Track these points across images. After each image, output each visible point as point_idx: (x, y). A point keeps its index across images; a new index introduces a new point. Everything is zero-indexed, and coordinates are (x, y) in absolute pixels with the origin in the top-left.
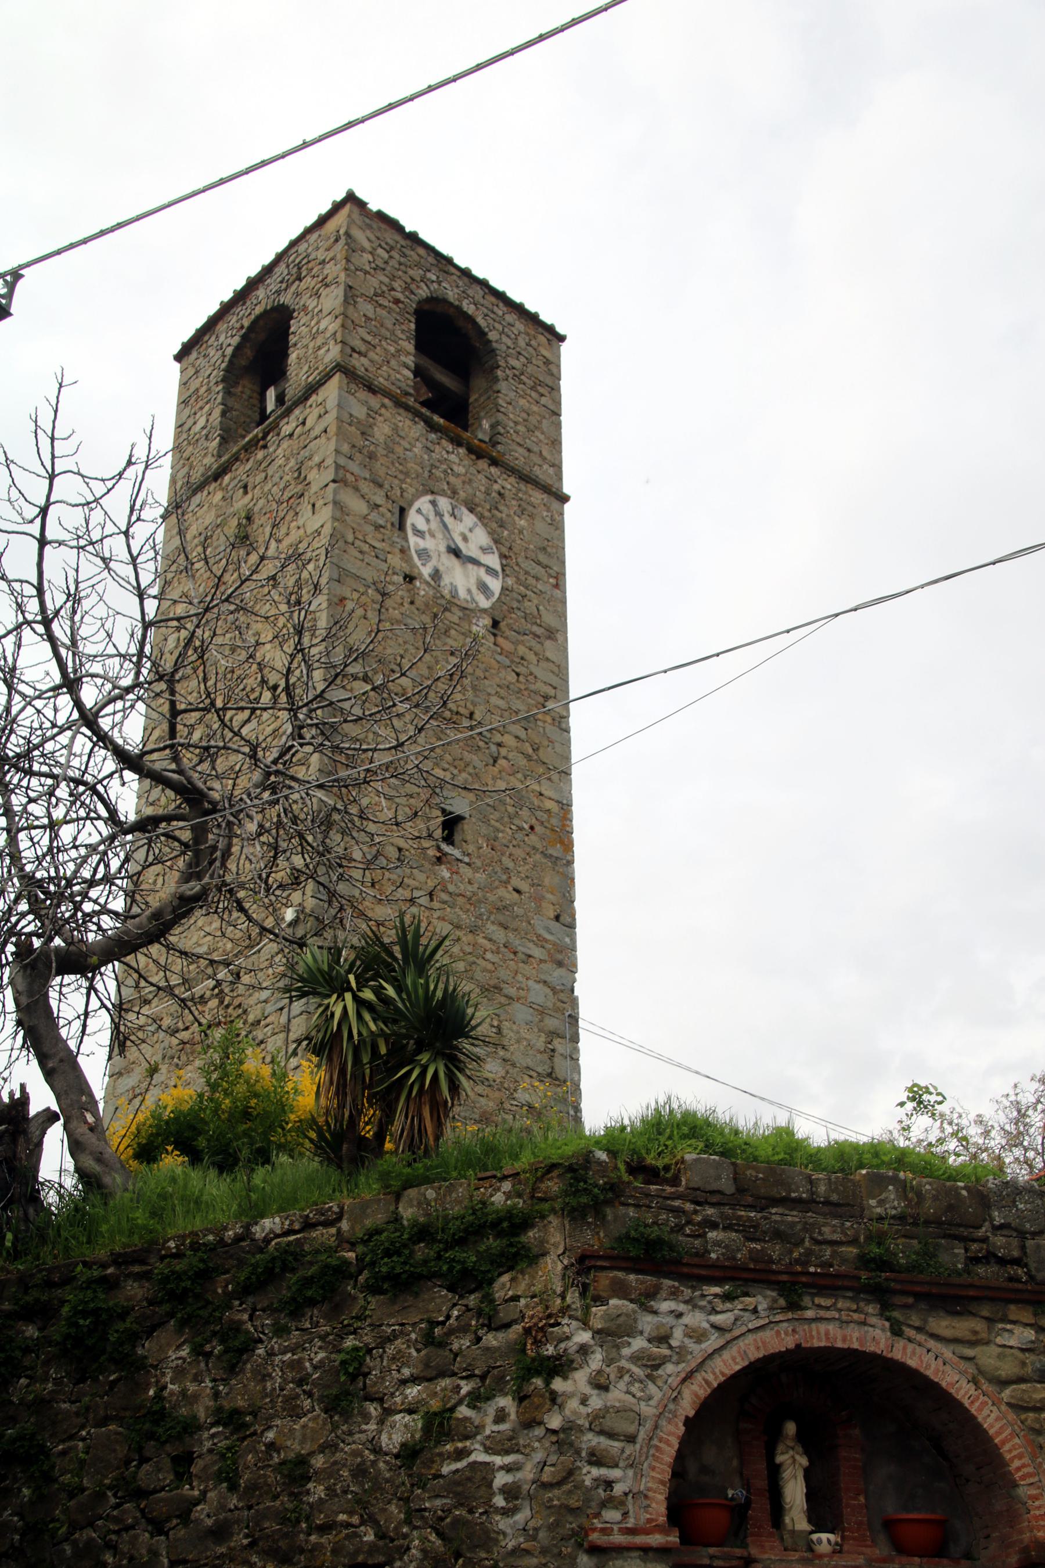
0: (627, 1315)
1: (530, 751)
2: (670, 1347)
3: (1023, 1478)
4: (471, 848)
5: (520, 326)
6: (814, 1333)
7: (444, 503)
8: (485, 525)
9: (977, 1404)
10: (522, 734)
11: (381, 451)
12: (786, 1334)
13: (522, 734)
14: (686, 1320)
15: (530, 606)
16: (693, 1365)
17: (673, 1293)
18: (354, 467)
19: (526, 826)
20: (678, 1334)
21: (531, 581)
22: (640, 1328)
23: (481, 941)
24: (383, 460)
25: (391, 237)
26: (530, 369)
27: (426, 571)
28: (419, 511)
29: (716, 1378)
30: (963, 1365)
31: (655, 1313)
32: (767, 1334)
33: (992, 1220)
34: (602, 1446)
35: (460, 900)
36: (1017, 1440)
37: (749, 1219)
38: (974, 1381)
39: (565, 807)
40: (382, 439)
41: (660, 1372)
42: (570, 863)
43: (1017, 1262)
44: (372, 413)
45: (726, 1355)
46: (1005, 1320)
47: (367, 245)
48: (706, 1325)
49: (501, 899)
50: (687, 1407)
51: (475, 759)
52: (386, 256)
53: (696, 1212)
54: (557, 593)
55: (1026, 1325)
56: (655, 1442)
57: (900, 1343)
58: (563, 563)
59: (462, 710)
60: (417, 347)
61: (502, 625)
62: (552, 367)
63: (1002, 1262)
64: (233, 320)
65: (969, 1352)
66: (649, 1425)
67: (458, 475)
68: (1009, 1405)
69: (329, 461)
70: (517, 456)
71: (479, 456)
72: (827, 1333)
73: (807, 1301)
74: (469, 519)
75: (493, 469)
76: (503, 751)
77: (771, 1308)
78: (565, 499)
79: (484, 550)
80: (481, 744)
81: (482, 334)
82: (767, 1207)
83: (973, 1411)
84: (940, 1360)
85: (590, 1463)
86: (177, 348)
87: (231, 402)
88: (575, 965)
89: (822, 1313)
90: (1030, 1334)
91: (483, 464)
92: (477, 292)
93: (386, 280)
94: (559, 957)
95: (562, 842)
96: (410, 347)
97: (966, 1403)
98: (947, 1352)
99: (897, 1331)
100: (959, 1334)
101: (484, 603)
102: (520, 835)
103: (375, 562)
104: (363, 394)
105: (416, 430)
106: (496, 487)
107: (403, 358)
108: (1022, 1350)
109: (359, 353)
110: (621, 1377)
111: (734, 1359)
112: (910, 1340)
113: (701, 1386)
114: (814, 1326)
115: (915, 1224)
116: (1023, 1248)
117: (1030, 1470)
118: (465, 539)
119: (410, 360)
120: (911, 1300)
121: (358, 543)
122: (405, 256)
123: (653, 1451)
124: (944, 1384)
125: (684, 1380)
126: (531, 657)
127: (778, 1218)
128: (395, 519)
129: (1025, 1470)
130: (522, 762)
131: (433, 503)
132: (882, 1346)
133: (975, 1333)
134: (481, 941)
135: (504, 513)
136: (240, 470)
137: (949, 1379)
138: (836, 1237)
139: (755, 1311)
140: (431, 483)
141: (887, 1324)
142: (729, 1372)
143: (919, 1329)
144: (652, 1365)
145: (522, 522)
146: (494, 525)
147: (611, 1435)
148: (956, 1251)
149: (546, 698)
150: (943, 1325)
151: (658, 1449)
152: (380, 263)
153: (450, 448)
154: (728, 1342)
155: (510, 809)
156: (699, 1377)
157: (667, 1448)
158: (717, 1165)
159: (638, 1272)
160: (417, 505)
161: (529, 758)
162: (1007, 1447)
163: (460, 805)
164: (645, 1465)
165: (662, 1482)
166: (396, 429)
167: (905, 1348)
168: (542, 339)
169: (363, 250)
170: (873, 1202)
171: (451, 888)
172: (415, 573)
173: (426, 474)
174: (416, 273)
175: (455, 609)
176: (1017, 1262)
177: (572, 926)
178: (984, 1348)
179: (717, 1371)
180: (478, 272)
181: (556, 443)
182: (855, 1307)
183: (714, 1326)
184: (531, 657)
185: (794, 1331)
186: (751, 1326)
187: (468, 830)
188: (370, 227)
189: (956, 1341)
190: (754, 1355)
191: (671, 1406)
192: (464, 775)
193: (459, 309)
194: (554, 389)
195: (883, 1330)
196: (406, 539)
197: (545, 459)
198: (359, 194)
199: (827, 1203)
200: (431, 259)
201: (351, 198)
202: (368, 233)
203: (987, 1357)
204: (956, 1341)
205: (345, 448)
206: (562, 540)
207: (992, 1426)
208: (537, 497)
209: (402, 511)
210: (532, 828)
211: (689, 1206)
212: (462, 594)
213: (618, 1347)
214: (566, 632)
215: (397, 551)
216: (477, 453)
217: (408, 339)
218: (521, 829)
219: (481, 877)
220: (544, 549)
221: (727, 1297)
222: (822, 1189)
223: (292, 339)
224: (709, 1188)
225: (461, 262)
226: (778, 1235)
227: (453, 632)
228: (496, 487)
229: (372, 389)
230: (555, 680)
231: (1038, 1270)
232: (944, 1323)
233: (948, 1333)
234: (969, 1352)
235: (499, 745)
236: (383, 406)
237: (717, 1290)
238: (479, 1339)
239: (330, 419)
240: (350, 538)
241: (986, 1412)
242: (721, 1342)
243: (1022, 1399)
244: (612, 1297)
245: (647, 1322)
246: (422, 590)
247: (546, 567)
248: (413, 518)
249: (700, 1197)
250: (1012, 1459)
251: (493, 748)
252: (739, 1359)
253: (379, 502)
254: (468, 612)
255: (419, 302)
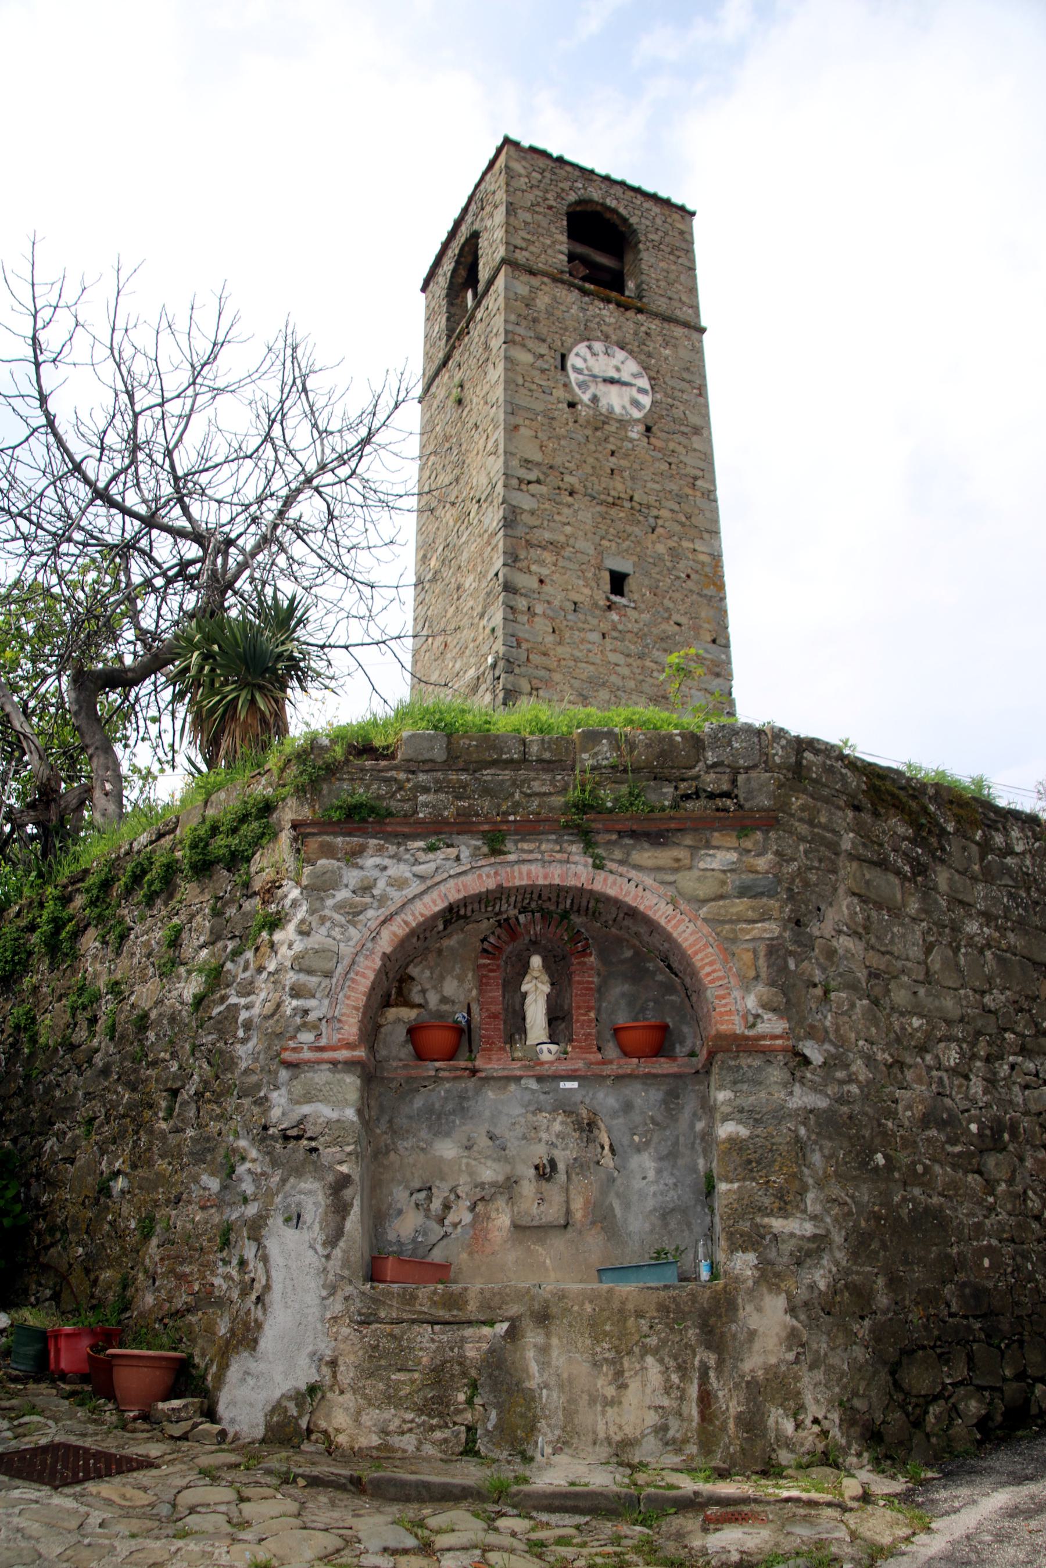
0: (333, 872)
1: (684, 519)
2: (373, 896)
3: (712, 981)
4: (636, 597)
5: (656, 210)
6: (516, 874)
7: (598, 346)
8: (635, 358)
9: (673, 922)
10: (676, 507)
11: (543, 316)
12: (488, 876)
13: (676, 507)
14: (389, 872)
15: (677, 413)
16: (393, 909)
17: (379, 850)
18: (520, 330)
19: (683, 576)
20: (381, 884)
21: (678, 394)
22: (345, 882)
23: (648, 663)
24: (543, 322)
25: (542, 162)
26: (667, 239)
27: (586, 398)
28: (577, 355)
29: (415, 918)
30: (662, 890)
31: (362, 868)
32: (468, 879)
33: (706, 759)
34: (301, 981)
35: (629, 636)
36: (710, 950)
37: (459, 781)
38: (673, 902)
39: (717, 559)
40: (543, 308)
41: (361, 917)
42: (723, 599)
43: (727, 795)
44: (533, 290)
45: (427, 899)
46: (708, 846)
47: (522, 171)
48: (408, 875)
49: (664, 632)
50: (386, 943)
51: (636, 530)
52: (539, 177)
53: (408, 780)
54: (701, 400)
55: (729, 849)
56: (352, 975)
57: (601, 875)
58: (704, 377)
59: (622, 495)
60: (569, 237)
61: (654, 429)
62: (687, 236)
63: (712, 796)
64: (450, 253)
65: (670, 878)
66: (346, 962)
67: (609, 325)
68: (704, 920)
69: (502, 330)
70: (660, 304)
71: (627, 309)
72: (529, 873)
73: (510, 846)
74: (620, 355)
75: (639, 316)
76: (660, 522)
77: (473, 855)
78: (703, 330)
79: (635, 376)
80: (641, 518)
81: (625, 220)
82: (480, 770)
83: (669, 928)
84: (640, 888)
85: (292, 997)
86: (421, 283)
87: (453, 311)
88: (731, 674)
89: (525, 856)
90: (733, 856)
91: (630, 314)
92: (618, 191)
93: (541, 194)
94: (717, 670)
95: (715, 584)
96: (564, 238)
97: (663, 922)
98: (648, 880)
99: (598, 866)
100: (661, 862)
101: (637, 414)
102: (677, 583)
103: (542, 396)
104: (525, 277)
105: (570, 298)
106: (643, 329)
107: (558, 247)
108: (724, 872)
109: (521, 249)
110: (323, 924)
111: (434, 902)
112: (611, 872)
113: (399, 927)
114: (516, 867)
115: (625, 771)
116: (734, 782)
117: (721, 974)
118: (618, 370)
119: (564, 248)
120: (614, 837)
121: (527, 384)
122: (555, 174)
123: (348, 983)
124: (642, 908)
125: (384, 922)
126: (681, 449)
127: (489, 778)
128: (558, 363)
129: (715, 975)
130: (677, 528)
131: (589, 347)
132: (583, 879)
133: (678, 860)
134: (648, 663)
135: (651, 347)
136: (456, 354)
137: (647, 903)
138: (545, 789)
139: (458, 858)
140: (587, 333)
141: (590, 861)
142: (428, 913)
143: (621, 862)
144: (353, 913)
145: (667, 352)
146: (643, 357)
147: (310, 972)
148: (665, 790)
149: (695, 478)
150: (646, 856)
151: (353, 980)
152: (534, 182)
153: (602, 306)
154: (429, 888)
155: (669, 564)
156: (398, 919)
157: (363, 980)
158: (431, 738)
159: (345, 835)
160: (575, 350)
161: (683, 525)
162: (699, 956)
163: (622, 565)
164: (341, 995)
165: (356, 1009)
166: (554, 299)
167: (605, 880)
168: (676, 217)
169: (520, 176)
170: (585, 756)
171: (620, 627)
172: (576, 400)
173: (582, 327)
174: (566, 185)
175: (612, 422)
176: (727, 795)
177: (727, 646)
178: (686, 873)
179: (417, 913)
180: (616, 176)
181: (693, 291)
182: (558, 848)
183: (415, 875)
184: (681, 449)
185: (496, 873)
186: (452, 872)
187: (631, 584)
188: (524, 159)
189: (659, 869)
190: (454, 896)
191: (369, 945)
192: (627, 543)
193: (603, 205)
194: (688, 251)
195: (585, 866)
196: (568, 376)
197: (684, 303)
198: (513, 136)
199: (540, 761)
200: (577, 173)
201: (507, 141)
202: (524, 163)
203: (687, 881)
204: (659, 869)
205: (513, 318)
206: (702, 360)
207: (686, 940)
208: (679, 331)
209: (564, 358)
210: (688, 576)
211: (402, 776)
212: (618, 410)
213: (322, 899)
214: (709, 428)
215: (560, 385)
216: (621, 306)
217: (562, 233)
218: (678, 578)
219: (646, 617)
220: (688, 369)
221: (432, 849)
222: (535, 749)
223: (480, 252)
224: (421, 758)
225: (601, 171)
226: (486, 791)
227: (612, 439)
228: (643, 329)
229: (532, 273)
230: (702, 465)
231: (746, 800)
232: (646, 855)
233: (650, 863)
234: (670, 878)
235: (657, 517)
236: (543, 283)
237: (421, 844)
238: (241, 906)
239: (501, 299)
240: (520, 381)
241: (682, 928)
242: (423, 887)
243: (718, 914)
244: (319, 858)
245: (352, 877)
246: (583, 411)
247: (689, 382)
248: (572, 360)
249: (412, 766)
250: (703, 967)
251: (652, 521)
252: (439, 901)
253: (543, 352)
254: (624, 423)
255: (570, 206)
